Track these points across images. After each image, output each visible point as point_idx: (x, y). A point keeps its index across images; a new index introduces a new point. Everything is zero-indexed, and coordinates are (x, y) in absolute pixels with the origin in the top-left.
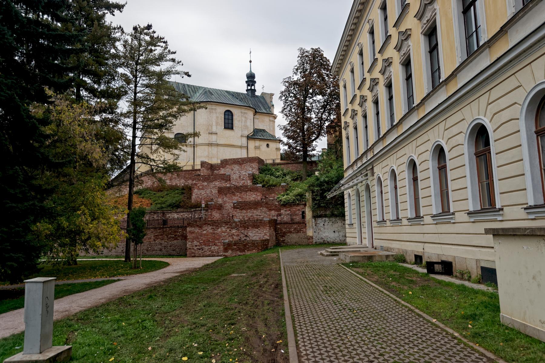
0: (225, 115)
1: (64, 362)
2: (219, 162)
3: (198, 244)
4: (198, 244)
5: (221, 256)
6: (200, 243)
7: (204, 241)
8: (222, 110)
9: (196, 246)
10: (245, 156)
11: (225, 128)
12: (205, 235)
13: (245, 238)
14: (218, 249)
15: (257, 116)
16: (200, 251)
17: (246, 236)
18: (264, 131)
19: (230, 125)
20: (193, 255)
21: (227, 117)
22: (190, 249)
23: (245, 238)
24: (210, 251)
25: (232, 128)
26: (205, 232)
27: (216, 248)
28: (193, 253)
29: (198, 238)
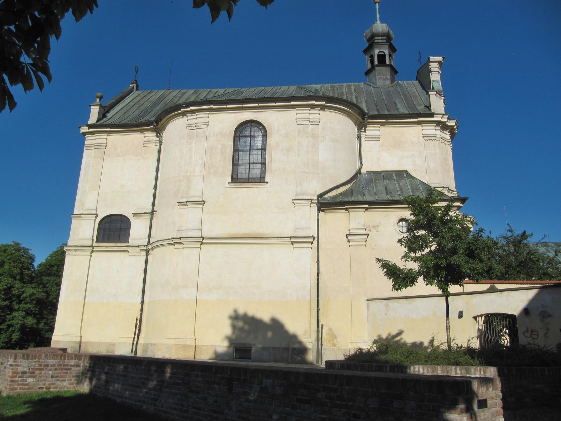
15: (373, 130)
25: (235, 179)
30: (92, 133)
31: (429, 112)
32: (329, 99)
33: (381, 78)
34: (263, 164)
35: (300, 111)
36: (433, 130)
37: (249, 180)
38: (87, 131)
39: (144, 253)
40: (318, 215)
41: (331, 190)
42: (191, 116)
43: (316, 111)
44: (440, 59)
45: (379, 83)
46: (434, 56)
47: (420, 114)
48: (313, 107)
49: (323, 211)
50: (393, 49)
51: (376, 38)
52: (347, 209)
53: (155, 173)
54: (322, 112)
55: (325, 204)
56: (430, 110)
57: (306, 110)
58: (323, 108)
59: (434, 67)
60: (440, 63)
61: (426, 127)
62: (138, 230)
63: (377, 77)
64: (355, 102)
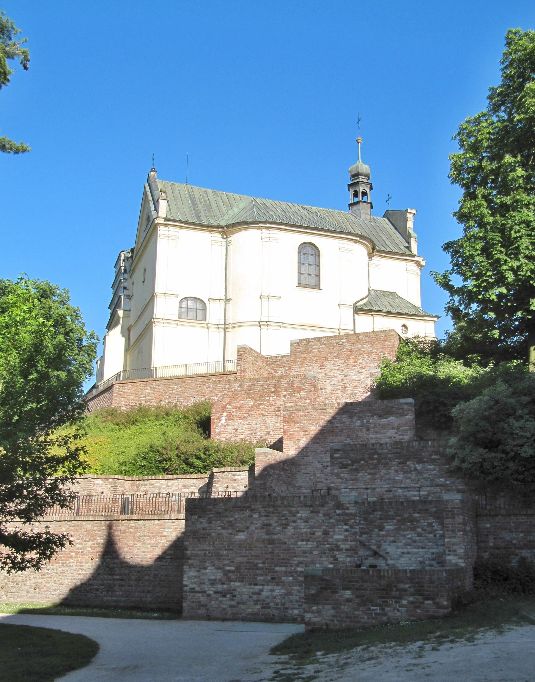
0: (299, 253)
1: (534, 168)
2: (286, 350)
3: (219, 575)
4: (219, 575)
5: (293, 620)
6: (226, 573)
7: (238, 569)
8: (295, 239)
9: (213, 583)
10: (184, 521)
11: (300, 285)
12: (241, 545)
13: (371, 561)
14: (283, 596)
15: (376, 260)
16: (226, 602)
17: (375, 554)
18: (394, 294)
19: (312, 281)
20: (202, 612)
21: (304, 270)
22: (192, 590)
23: (371, 561)
24: (256, 602)
25: (318, 287)
26: (241, 536)
27: (279, 591)
28: (202, 606)
29: (219, 557)
30: (166, 225)
31: (410, 253)
32: (362, 237)
33: (363, 213)
34: (299, 273)
35: (342, 241)
36: (413, 266)
37: (309, 286)
38: (163, 222)
39: (222, 331)
40: (354, 316)
41: (361, 300)
42: (264, 231)
43: (352, 243)
44: (414, 212)
45: (363, 216)
46: (413, 208)
47: (405, 254)
48: (350, 240)
49: (357, 314)
50: (371, 188)
51: (360, 176)
52: (372, 315)
53: (225, 270)
54: (354, 244)
55: (358, 310)
56: (411, 251)
57: (346, 242)
58: (356, 242)
59: (410, 216)
60: (414, 214)
61: (409, 263)
62: (215, 313)
63: (362, 211)
64: (353, 232)
